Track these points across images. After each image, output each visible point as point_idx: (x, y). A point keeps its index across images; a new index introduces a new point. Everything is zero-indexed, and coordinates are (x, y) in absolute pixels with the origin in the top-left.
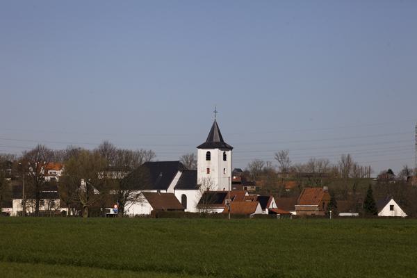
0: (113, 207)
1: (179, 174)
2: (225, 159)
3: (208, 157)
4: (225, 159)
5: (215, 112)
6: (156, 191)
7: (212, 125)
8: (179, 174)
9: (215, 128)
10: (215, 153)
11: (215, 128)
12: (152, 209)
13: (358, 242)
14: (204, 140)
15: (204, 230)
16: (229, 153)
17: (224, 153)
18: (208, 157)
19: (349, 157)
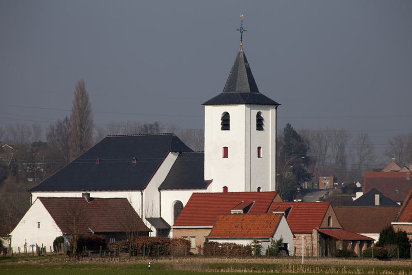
0: (371, 273)
1: (171, 159)
2: (260, 125)
3: (226, 123)
4: (260, 125)
5: (242, 30)
6: (79, 195)
7: (234, 60)
8: (171, 159)
9: (242, 66)
10: (239, 113)
11: (242, 66)
12: (58, 233)
13: (252, 224)
14: (219, 90)
15: (337, 261)
16: (269, 115)
17: (259, 115)
18: (226, 123)
19: (289, 125)
